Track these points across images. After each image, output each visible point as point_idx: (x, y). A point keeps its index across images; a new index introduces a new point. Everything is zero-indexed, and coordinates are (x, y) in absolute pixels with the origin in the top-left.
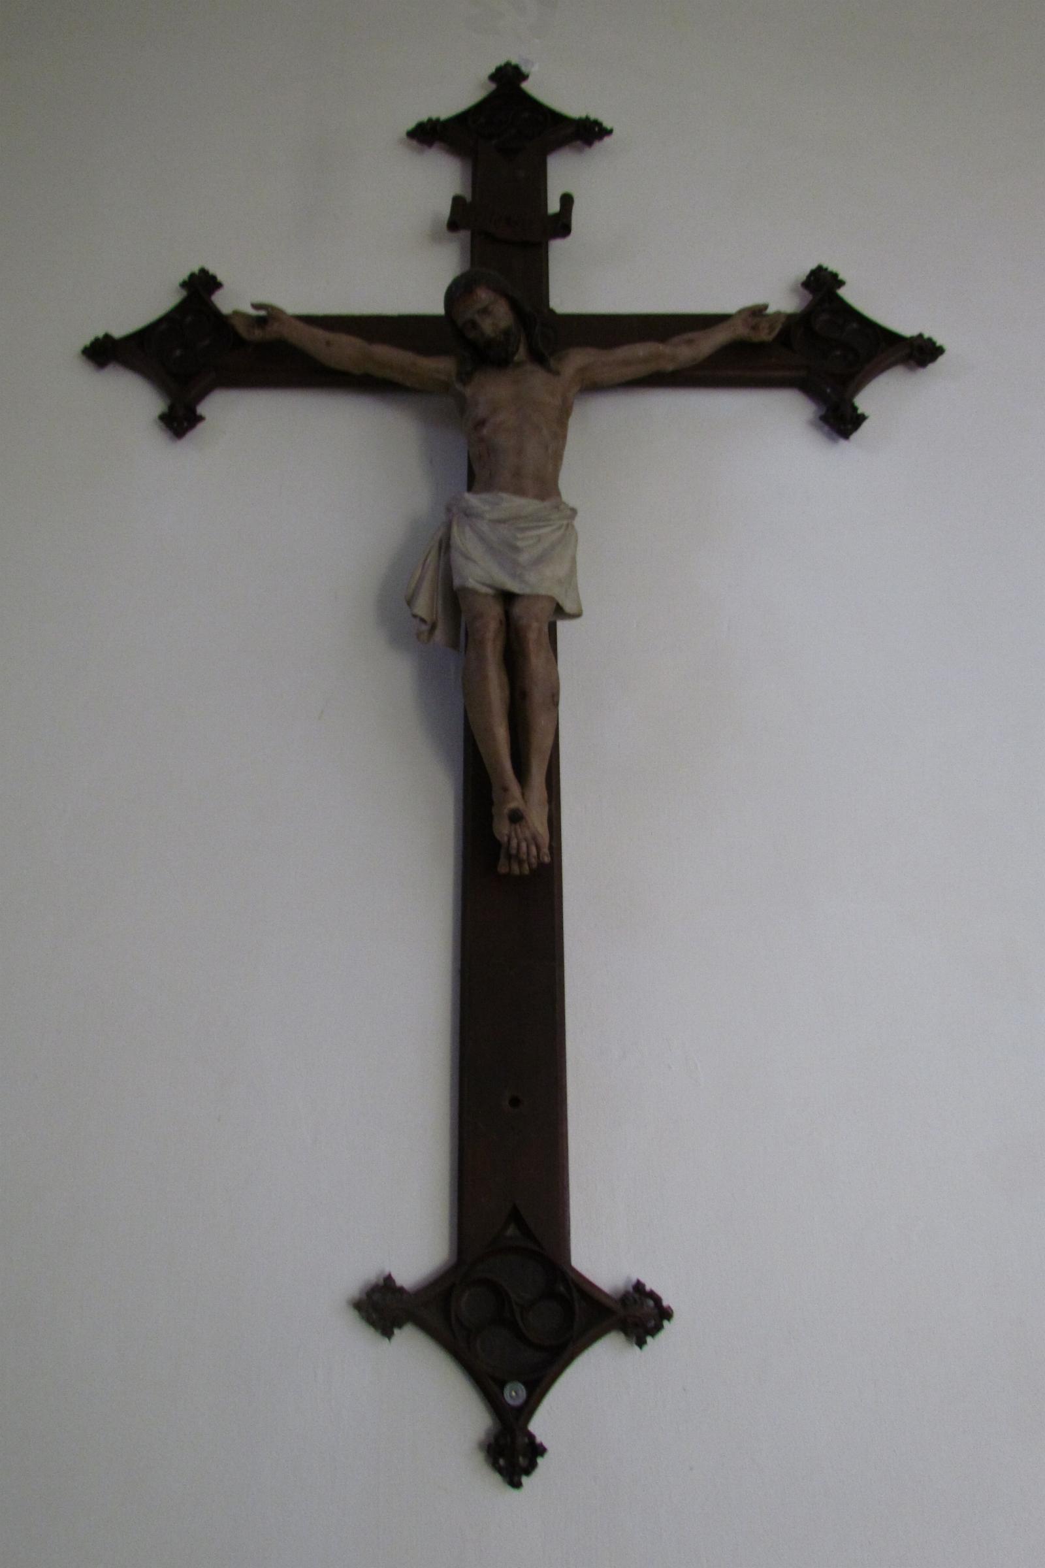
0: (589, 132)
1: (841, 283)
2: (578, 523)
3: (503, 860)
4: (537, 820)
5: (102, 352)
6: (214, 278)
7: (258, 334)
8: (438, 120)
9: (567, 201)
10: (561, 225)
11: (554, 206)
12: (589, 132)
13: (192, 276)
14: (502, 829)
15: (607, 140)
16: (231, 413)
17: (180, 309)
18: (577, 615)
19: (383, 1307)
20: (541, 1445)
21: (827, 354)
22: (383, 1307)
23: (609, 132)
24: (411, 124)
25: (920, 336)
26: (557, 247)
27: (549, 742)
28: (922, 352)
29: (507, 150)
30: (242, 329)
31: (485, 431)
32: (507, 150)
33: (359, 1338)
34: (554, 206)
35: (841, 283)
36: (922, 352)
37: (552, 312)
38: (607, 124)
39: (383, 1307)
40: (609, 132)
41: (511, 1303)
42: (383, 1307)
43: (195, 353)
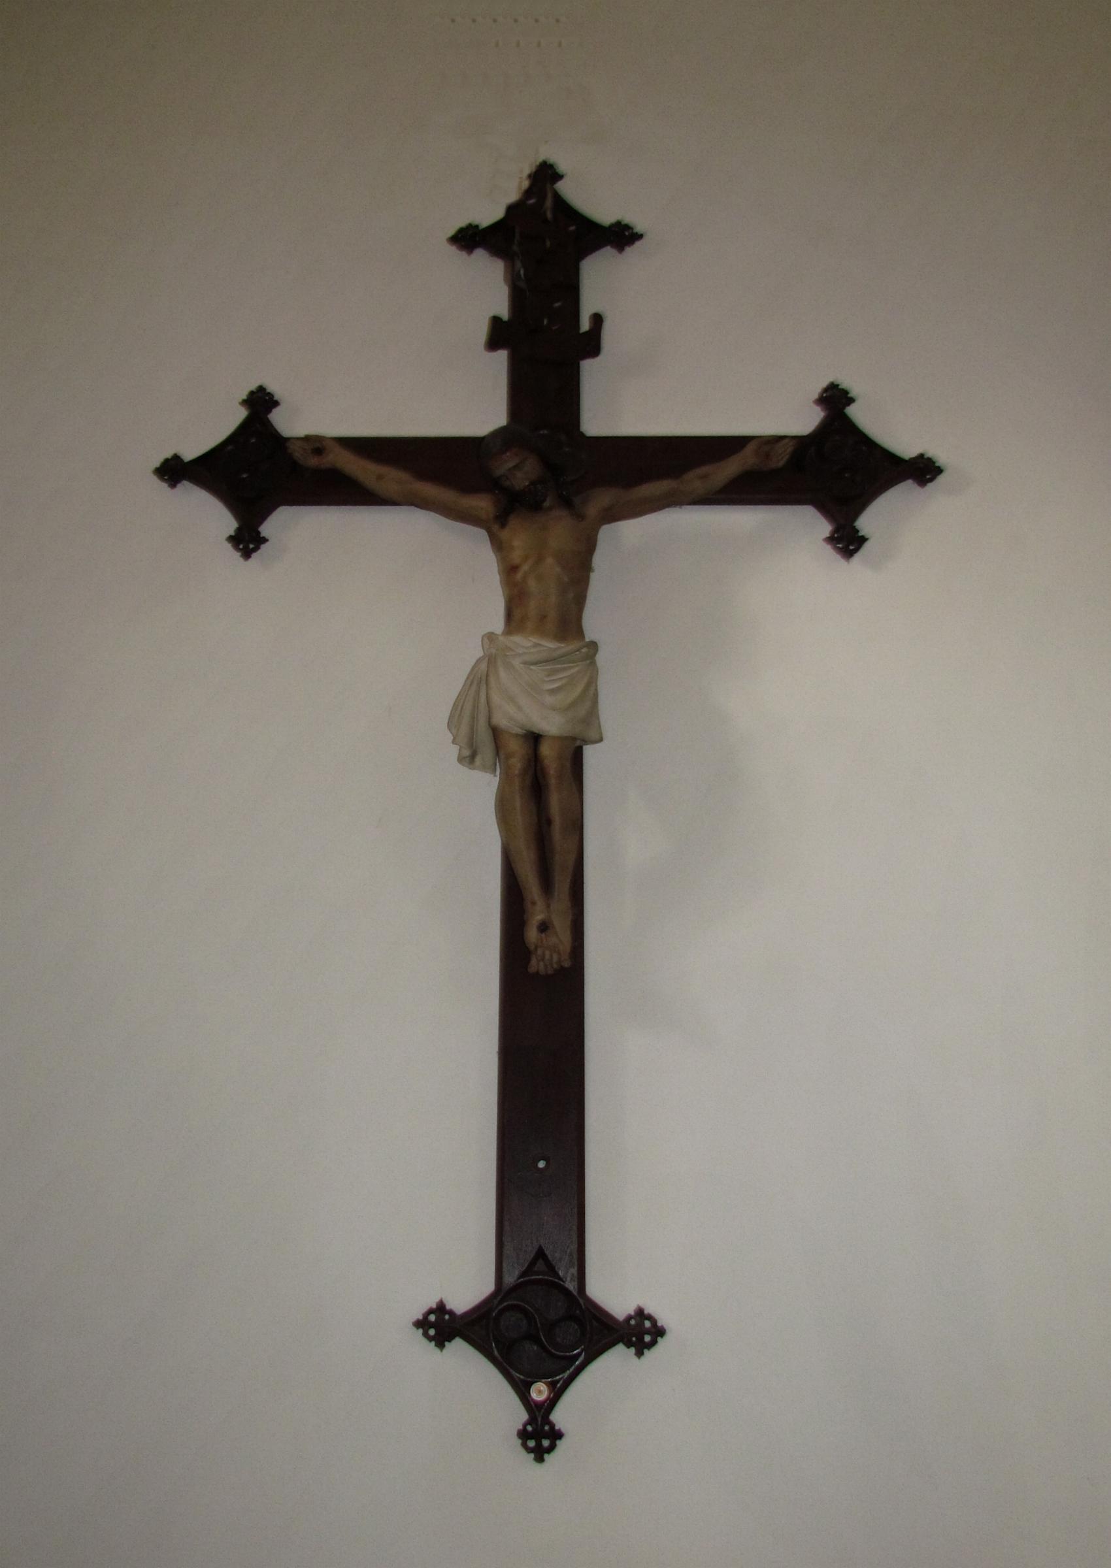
0: (622, 236)
1: (851, 400)
2: (600, 658)
3: (534, 961)
4: (562, 936)
5: (173, 471)
6: (271, 395)
7: (313, 462)
8: (477, 226)
9: (597, 319)
10: (591, 344)
11: (585, 325)
12: (622, 236)
13: (252, 393)
14: (532, 935)
15: (638, 244)
16: (295, 528)
17: (244, 429)
18: (601, 740)
19: (261, 403)
20: (559, 1430)
21: (836, 473)
22: (440, 1326)
23: (638, 237)
24: (452, 232)
25: (921, 456)
26: (588, 367)
27: (571, 859)
28: (924, 470)
29: (545, 250)
30: (297, 452)
31: (519, 576)
32: (545, 250)
33: (421, 1348)
34: (585, 325)
35: (851, 400)
36: (924, 470)
37: (582, 434)
38: (639, 229)
39: (440, 1326)
40: (638, 237)
41: (540, 1324)
42: (261, 403)
43: (259, 473)
